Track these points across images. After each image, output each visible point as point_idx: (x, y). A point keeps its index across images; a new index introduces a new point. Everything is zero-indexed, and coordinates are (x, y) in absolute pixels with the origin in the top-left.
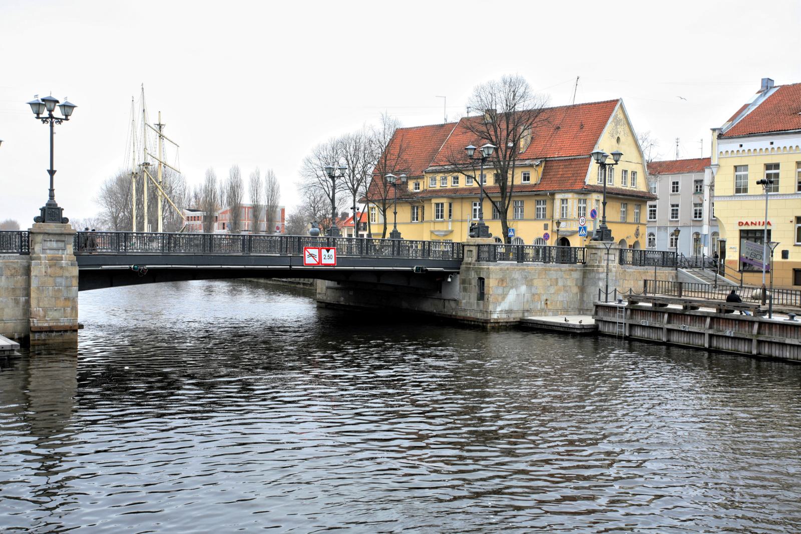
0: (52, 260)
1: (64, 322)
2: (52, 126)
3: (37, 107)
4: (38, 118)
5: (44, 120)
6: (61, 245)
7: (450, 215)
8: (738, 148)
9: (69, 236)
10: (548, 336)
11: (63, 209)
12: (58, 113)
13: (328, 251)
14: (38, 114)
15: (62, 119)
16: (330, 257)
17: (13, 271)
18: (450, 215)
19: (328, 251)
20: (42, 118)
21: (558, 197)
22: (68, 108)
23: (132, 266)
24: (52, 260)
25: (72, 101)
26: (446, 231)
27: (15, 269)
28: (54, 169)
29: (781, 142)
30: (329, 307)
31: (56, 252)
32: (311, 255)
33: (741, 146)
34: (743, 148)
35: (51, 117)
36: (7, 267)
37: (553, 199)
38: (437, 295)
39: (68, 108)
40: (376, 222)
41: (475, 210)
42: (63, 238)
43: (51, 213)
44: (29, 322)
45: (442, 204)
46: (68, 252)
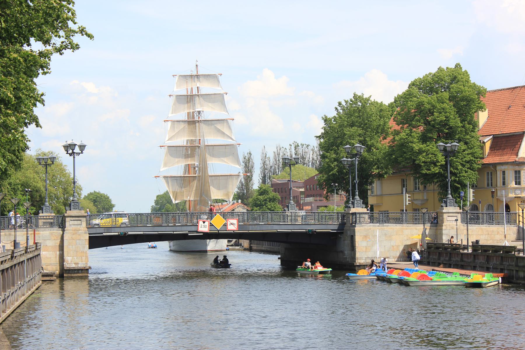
1: (81, 265)
2: (74, 158)
4: (67, 153)
5: (71, 155)
10: (248, 281)
12: (77, 150)
13: (204, 222)
14: (67, 152)
15: (79, 153)
16: (205, 227)
19: (204, 222)
22: (82, 148)
25: (84, 143)
26: (422, 200)
30: (468, 286)
32: (232, 224)
35: (73, 153)
39: (82, 148)
40: (375, 194)
44: (63, 265)
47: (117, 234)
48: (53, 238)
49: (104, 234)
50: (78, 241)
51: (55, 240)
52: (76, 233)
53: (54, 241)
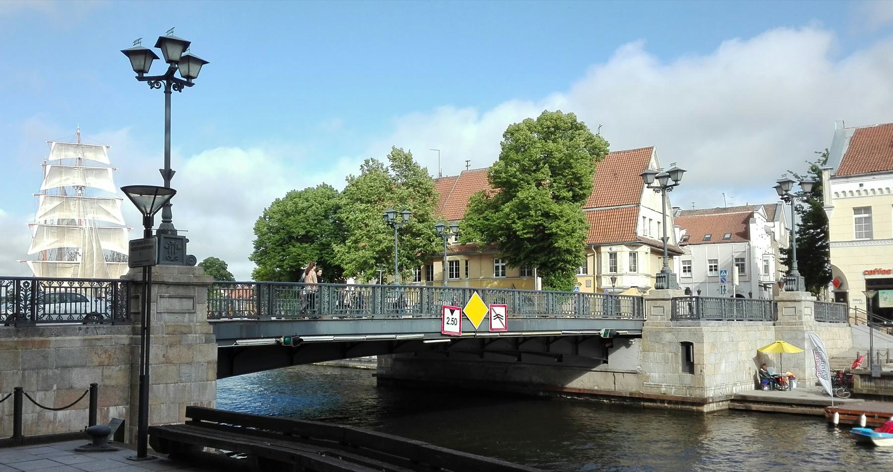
0: (173, 333)
3: (139, 57)
4: (141, 78)
5: (154, 81)
6: (187, 304)
7: (467, 274)
8: (858, 188)
9: (200, 288)
11: (188, 241)
13: (452, 312)
17: (104, 356)
18: (467, 274)
19: (452, 312)
20: (149, 79)
21: (605, 250)
23: (282, 339)
24: (173, 333)
27: (106, 351)
28: (172, 168)
29: (871, 183)
31: (180, 317)
33: (861, 185)
34: (864, 188)
36: (190, 346)
37: (599, 253)
38: (602, 366)
41: (497, 268)
42: (191, 292)
43: (158, 248)
45: (457, 262)
46: (199, 319)
47: (272, 341)
48: (96, 360)
49: (241, 343)
50: (185, 369)
51: (101, 365)
52: (180, 342)
53: (99, 371)
